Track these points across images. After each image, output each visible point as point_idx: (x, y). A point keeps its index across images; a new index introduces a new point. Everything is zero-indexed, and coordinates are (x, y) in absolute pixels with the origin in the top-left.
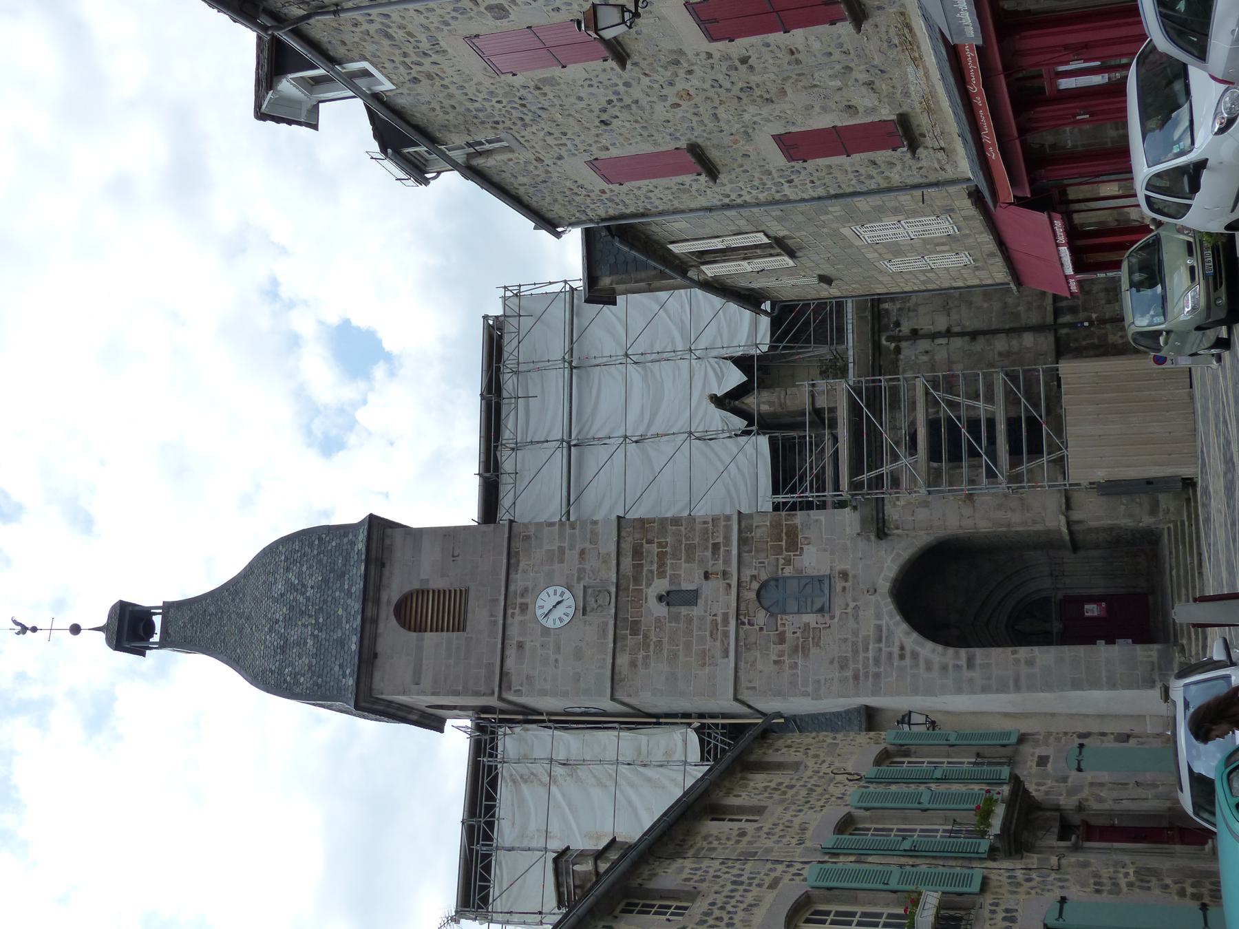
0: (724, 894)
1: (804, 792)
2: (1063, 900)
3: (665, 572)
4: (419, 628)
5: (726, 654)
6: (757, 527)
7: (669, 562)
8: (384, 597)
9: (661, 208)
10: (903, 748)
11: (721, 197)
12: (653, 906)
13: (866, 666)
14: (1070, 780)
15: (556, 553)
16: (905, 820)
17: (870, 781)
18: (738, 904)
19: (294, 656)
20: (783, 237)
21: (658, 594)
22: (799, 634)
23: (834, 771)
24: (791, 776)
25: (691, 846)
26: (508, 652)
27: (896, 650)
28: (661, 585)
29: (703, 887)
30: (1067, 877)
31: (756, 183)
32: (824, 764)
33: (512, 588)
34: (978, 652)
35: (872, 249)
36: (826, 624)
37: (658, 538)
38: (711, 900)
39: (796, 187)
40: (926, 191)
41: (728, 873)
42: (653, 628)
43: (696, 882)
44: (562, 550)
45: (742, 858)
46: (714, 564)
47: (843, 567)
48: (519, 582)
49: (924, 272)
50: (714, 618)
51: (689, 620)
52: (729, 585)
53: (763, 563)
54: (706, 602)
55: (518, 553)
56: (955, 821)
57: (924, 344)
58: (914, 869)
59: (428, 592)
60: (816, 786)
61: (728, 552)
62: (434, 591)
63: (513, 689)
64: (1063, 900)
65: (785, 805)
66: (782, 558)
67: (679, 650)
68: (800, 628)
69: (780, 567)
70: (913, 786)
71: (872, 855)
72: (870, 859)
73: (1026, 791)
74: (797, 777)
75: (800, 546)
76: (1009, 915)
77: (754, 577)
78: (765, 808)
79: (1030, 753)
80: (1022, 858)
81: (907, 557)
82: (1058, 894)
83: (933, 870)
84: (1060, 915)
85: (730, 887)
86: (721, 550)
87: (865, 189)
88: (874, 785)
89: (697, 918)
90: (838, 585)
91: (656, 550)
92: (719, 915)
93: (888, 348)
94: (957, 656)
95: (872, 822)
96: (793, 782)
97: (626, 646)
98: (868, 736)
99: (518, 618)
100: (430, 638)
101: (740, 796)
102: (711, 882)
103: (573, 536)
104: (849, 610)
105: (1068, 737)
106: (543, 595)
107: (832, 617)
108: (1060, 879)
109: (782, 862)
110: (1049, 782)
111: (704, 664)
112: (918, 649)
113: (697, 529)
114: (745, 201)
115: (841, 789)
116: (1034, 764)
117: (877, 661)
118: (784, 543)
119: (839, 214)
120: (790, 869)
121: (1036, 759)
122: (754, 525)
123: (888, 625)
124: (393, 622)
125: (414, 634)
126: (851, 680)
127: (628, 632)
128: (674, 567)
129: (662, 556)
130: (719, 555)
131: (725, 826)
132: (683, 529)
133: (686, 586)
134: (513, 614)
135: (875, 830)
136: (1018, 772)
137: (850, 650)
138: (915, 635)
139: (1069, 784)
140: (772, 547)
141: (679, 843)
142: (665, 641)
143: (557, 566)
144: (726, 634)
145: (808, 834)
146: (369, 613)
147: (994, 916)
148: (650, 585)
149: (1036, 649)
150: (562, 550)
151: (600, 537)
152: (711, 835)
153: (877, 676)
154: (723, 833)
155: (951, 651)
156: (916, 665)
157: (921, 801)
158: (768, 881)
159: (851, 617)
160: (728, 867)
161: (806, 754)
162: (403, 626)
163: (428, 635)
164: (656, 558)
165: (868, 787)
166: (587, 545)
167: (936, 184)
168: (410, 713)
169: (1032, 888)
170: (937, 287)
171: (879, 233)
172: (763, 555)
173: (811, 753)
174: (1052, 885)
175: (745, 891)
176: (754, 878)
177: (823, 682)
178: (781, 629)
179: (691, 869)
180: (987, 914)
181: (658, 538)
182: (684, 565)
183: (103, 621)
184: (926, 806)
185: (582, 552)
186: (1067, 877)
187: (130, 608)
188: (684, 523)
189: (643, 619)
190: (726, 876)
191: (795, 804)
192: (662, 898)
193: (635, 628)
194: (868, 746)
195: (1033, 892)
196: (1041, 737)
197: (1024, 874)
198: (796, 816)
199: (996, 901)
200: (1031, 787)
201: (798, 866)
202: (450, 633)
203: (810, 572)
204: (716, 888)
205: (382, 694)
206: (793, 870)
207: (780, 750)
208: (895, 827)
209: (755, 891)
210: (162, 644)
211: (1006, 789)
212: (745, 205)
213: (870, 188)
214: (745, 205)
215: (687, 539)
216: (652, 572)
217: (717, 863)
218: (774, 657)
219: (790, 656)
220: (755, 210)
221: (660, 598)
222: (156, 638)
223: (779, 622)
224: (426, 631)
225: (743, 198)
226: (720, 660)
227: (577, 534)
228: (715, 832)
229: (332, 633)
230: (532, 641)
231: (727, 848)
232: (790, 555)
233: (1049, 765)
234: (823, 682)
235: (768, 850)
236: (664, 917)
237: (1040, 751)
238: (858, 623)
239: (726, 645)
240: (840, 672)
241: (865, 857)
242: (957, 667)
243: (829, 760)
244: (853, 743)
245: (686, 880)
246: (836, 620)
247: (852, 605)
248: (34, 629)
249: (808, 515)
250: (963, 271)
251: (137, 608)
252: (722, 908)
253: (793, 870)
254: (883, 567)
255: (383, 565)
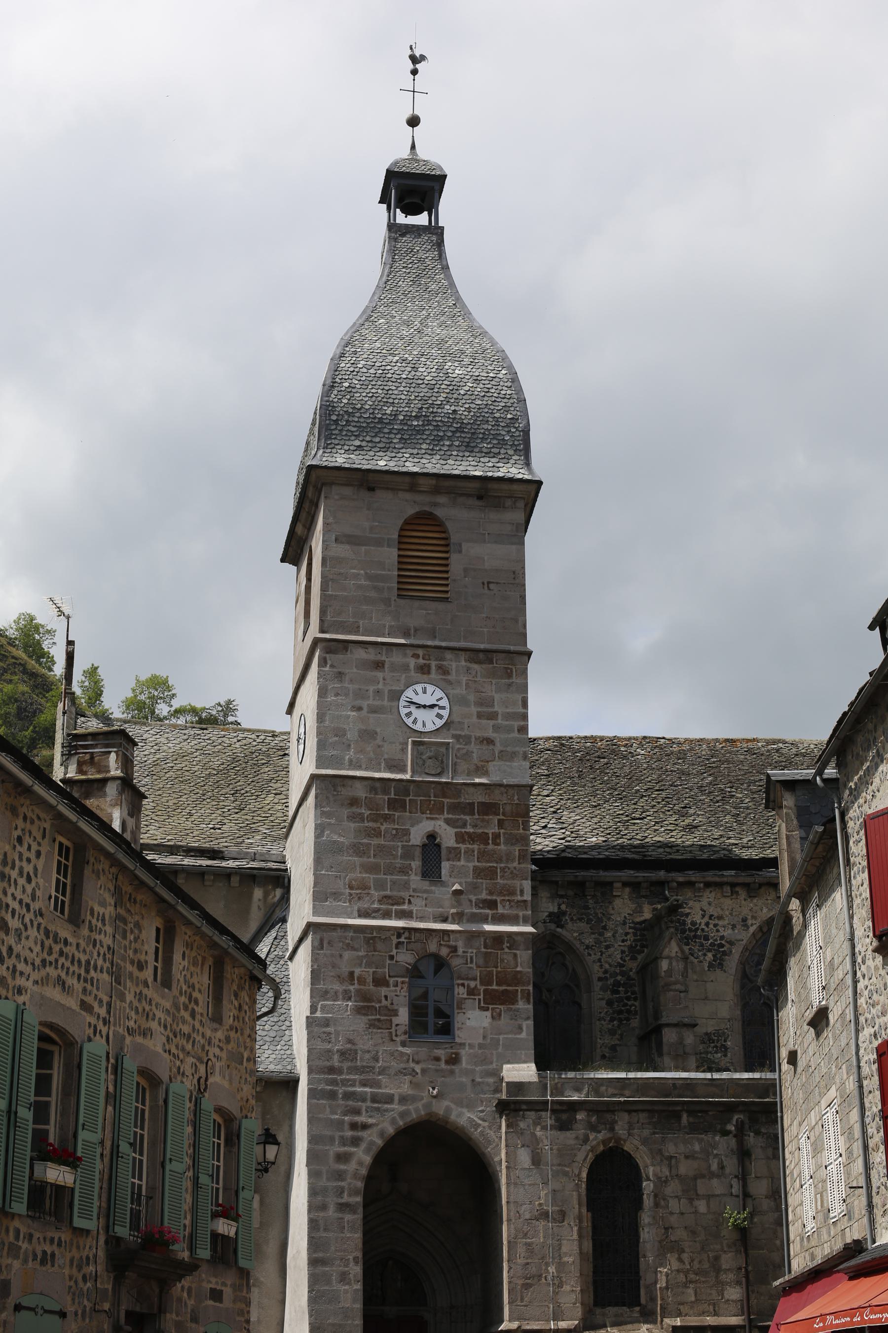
0: (76, 953)
1: (186, 1029)
2: (63, 1315)
3: (463, 842)
4: (402, 542)
5: (363, 914)
6: (515, 955)
7: (476, 847)
8: (442, 499)
9: (853, 882)
10: (235, 1138)
11: (863, 954)
12: (65, 877)
13: (345, 1082)
14: (194, 1325)
15: (490, 710)
16: (153, 1144)
17: (197, 1103)
18: (65, 970)
19: (373, 391)
20: (827, 1018)
21: (437, 833)
22: (384, 1002)
23: (210, 1062)
24: (205, 1015)
25: (129, 911)
26: (371, 650)
27: (362, 1119)
28: (448, 837)
29: (85, 932)
30: (87, 1320)
31: (875, 997)
32: (218, 1050)
33: (449, 655)
34: (357, 1217)
35: (818, 1118)
36: (396, 1035)
37: (504, 834)
38: (70, 940)
39: (871, 1043)
40: (863, 1191)
41: (99, 955)
42: (396, 827)
43: (90, 922)
44: (493, 716)
45: (114, 969)
46: (471, 901)
47: (464, 1060)
48: (456, 665)
49: (799, 1175)
50: (407, 901)
51: (405, 871)
52: (445, 920)
53: (472, 962)
54: (426, 891)
55: (491, 662)
56: (151, 1198)
57: (732, 1165)
58: (98, 1156)
59: (447, 552)
60: (194, 1042)
61: (485, 920)
62: (447, 559)
63: (328, 656)
64: (63, 1315)
65: (173, 1010)
66: (476, 985)
67: (369, 857)
68: (392, 1004)
69: (466, 982)
70: (191, 1151)
71: (115, 1110)
72: (110, 1108)
73: (180, 1278)
74: (204, 1020)
75: (491, 1007)
76: (49, 1257)
77: (454, 949)
78: (170, 988)
79: (226, 1282)
80: (107, 1271)
81: (473, 1137)
82: (70, 1309)
83: (97, 1174)
84: (46, 1311)
85: (84, 958)
86: (487, 911)
87: (867, 1120)
88: (193, 1108)
89: (51, 928)
90: (443, 1052)
91: (490, 832)
92: (54, 951)
93: (729, 1121)
94: (354, 1192)
95: (151, 1108)
96: (198, 1017)
97: (376, 794)
98: (250, 1098)
99: (412, 662)
100: (392, 554)
101: (184, 959)
102: (89, 937)
103: (509, 730)
104: (412, 1065)
105: (244, 1325)
106: (439, 693)
107: (403, 1044)
108: (85, 1311)
109: (109, 1012)
110: (192, 1302)
111: (351, 888)
112: (363, 1146)
113: (515, 882)
114: (859, 982)
115: (189, 1071)
116: (213, 1286)
117: (348, 1096)
118: (495, 987)
119: (848, 1087)
120: (101, 1022)
121: (219, 1288)
122: (518, 952)
123: (393, 1110)
124: (411, 511)
125: (396, 536)
126: (328, 1064)
127: (392, 796)
128: (469, 853)
129: (483, 838)
130: (482, 908)
131: (150, 945)
132: (516, 864)
133: (445, 866)
134: (416, 656)
135: (143, 1111)
136: (204, 1267)
137: (365, 1064)
138: (380, 1142)
139: (189, 1324)
140: (491, 973)
141: (133, 897)
142: (382, 842)
143: (474, 710)
144: (387, 915)
145: (139, 1039)
146: (422, 481)
147: (48, 1242)
148: (448, 824)
149: (359, 1286)
150: (493, 716)
151: (508, 763)
152: (140, 931)
153: (332, 1095)
154: (143, 944)
155: (360, 1185)
156: (343, 1142)
157: (173, 1162)
158: (89, 999)
159: (403, 1065)
160: (105, 954)
161: (231, 1028)
162: (406, 522)
163: (395, 552)
164: (480, 831)
165: (190, 1102)
166: (498, 747)
167: (870, 1206)
168: (304, 526)
169: (76, 1282)
170: (788, 1190)
171: (831, 1129)
172: (481, 962)
173: (232, 1034)
174: (79, 1303)
175: (79, 976)
176: (92, 985)
177: (328, 1029)
178: (392, 981)
179: (104, 914)
180: (49, 1234)
181: (504, 834)
182: (471, 865)
183: (423, 153)
184: (168, 1167)
185: (490, 741)
186: (87, 1320)
187: (437, 188)
188: (522, 866)
189: (408, 814)
190: (95, 954)
191: (173, 1021)
192: (74, 886)
193: (397, 804)
194: (239, 1098)
195: (72, 1283)
196: (244, 1293)
197: (91, 1273)
198: (160, 1024)
199: (63, 1244)
200: (186, 1282)
201: (104, 1030)
202: (396, 579)
203: (459, 1019)
204: (83, 944)
205: (326, 497)
206: (100, 1026)
207: (236, 999)
208: (146, 1133)
209: (78, 986)
210: (393, 227)
211: (185, 1255)
212: (855, 982)
213: (868, 1127)
214: (855, 982)
215: (503, 869)
216: (464, 825)
217: (110, 942)
218: (357, 971)
219: (358, 991)
220: (850, 992)
221: (432, 836)
222: (401, 218)
223: (400, 980)
224: (399, 549)
225: (861, 979)
226: (356, 908)
227: (511, 735)
228: (144, 935)
229: (399, 436)
230: (384, 679)
231: (126, 951)
232: (479, 995)
233: (211, 1303)
234: (328, 1029)
235: (122, 998)
236: (53, 893)
237: (228, 1292)
238: (396, 1075)
239: (373, 915)
240: (338, 1051)
241: (113, 1103)
242: (340, 1192)
243: (224, 1055)
244: (243, 1081)
245: (92, 910)
246: (400, 1049)
247: (418, 1069)
248: (414, 72)
249: (528, 1018)
250: (800, 1221)
251: (437, 195)
252: (61, 953)
253: (100, 1026)
254: (462, 1107)
255: (480, 498)
